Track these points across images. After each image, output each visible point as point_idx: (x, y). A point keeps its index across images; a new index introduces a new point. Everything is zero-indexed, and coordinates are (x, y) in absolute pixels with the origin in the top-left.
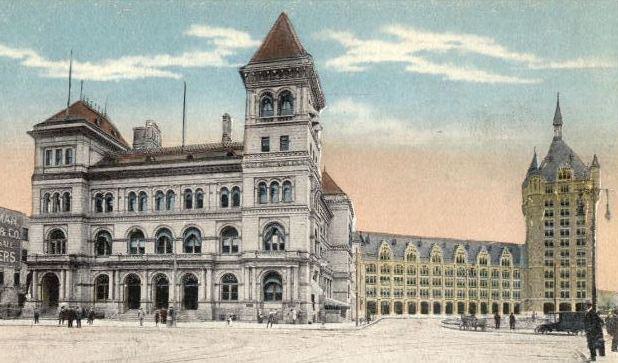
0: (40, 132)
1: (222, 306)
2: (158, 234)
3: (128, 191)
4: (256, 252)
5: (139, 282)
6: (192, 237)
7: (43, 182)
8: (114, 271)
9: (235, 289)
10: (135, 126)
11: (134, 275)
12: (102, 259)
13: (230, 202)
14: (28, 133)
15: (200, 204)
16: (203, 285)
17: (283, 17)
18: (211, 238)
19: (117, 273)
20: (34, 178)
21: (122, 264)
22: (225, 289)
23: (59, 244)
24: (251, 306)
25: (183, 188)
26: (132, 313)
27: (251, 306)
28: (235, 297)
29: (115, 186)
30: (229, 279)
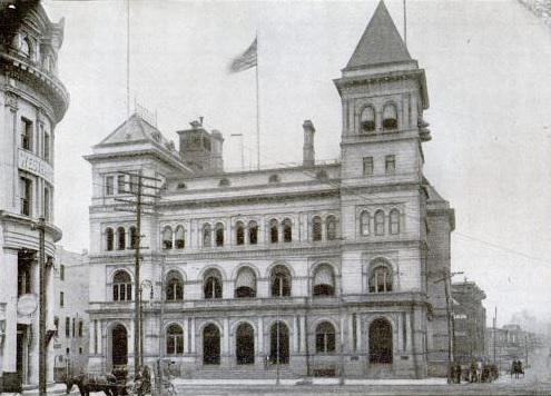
0: (341, 86)
1: (316, 358)
2: (205, 275)
3: (202, 222)
4: (306, 298)
5: (126, 332)
6: (280, 281)
7: (103, 215)
8: (190, 320)
9: (181, 341)
10: (313, 121)
11: (212, 325)
12: (174, 305)
13: (280, 235)
14: (85, 157)
15: (288, 237)
16: (296, 335)
17: (85, 157)
18: (301, 278)
19: (99, 324)
20: (92, 209)
21: (199, 311)
22: (170, 342)
23: (123, 286)
24: (357, 358)
25: (269, 218)
26: (211, 368)
27: (357, 358)
28: (180, 350)
29: (186, 217)
30: (175, 330)
